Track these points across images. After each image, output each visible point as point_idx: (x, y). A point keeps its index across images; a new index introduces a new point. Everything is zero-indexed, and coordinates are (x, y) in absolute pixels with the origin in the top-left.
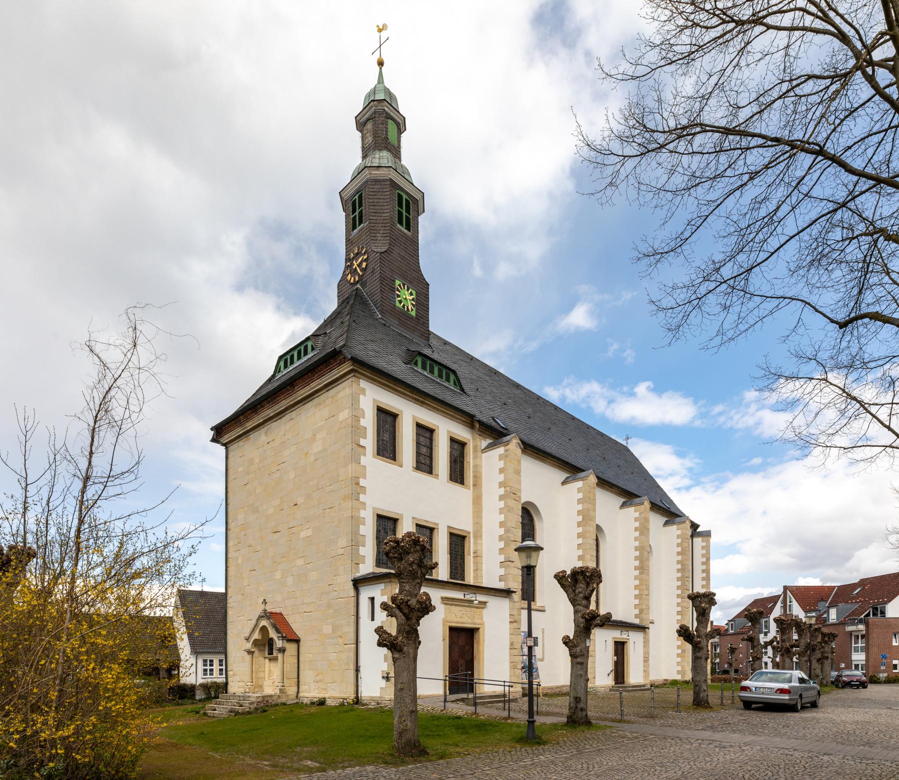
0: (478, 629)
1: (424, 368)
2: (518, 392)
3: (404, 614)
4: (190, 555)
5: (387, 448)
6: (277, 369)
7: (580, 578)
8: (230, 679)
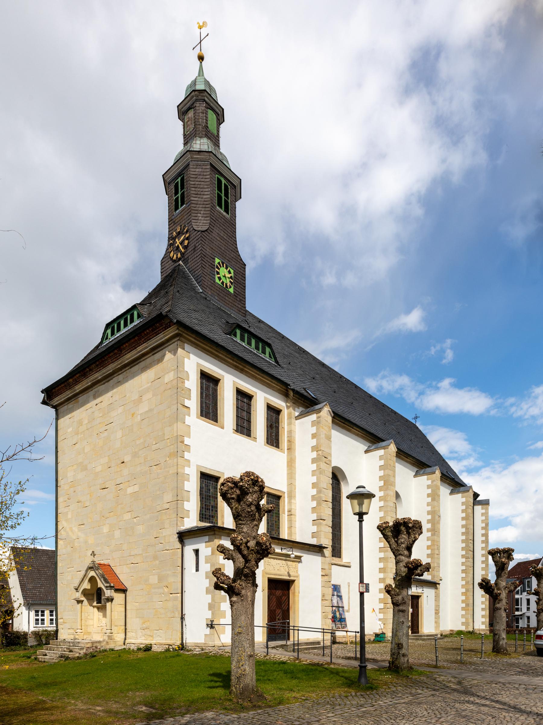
0: (293, 581)
1: (242, 339)
2: (323, 369)
3: (244, 556)
4: (18, 493)
5: (209, 410)
6: (105, 337)
7: (403, 528)
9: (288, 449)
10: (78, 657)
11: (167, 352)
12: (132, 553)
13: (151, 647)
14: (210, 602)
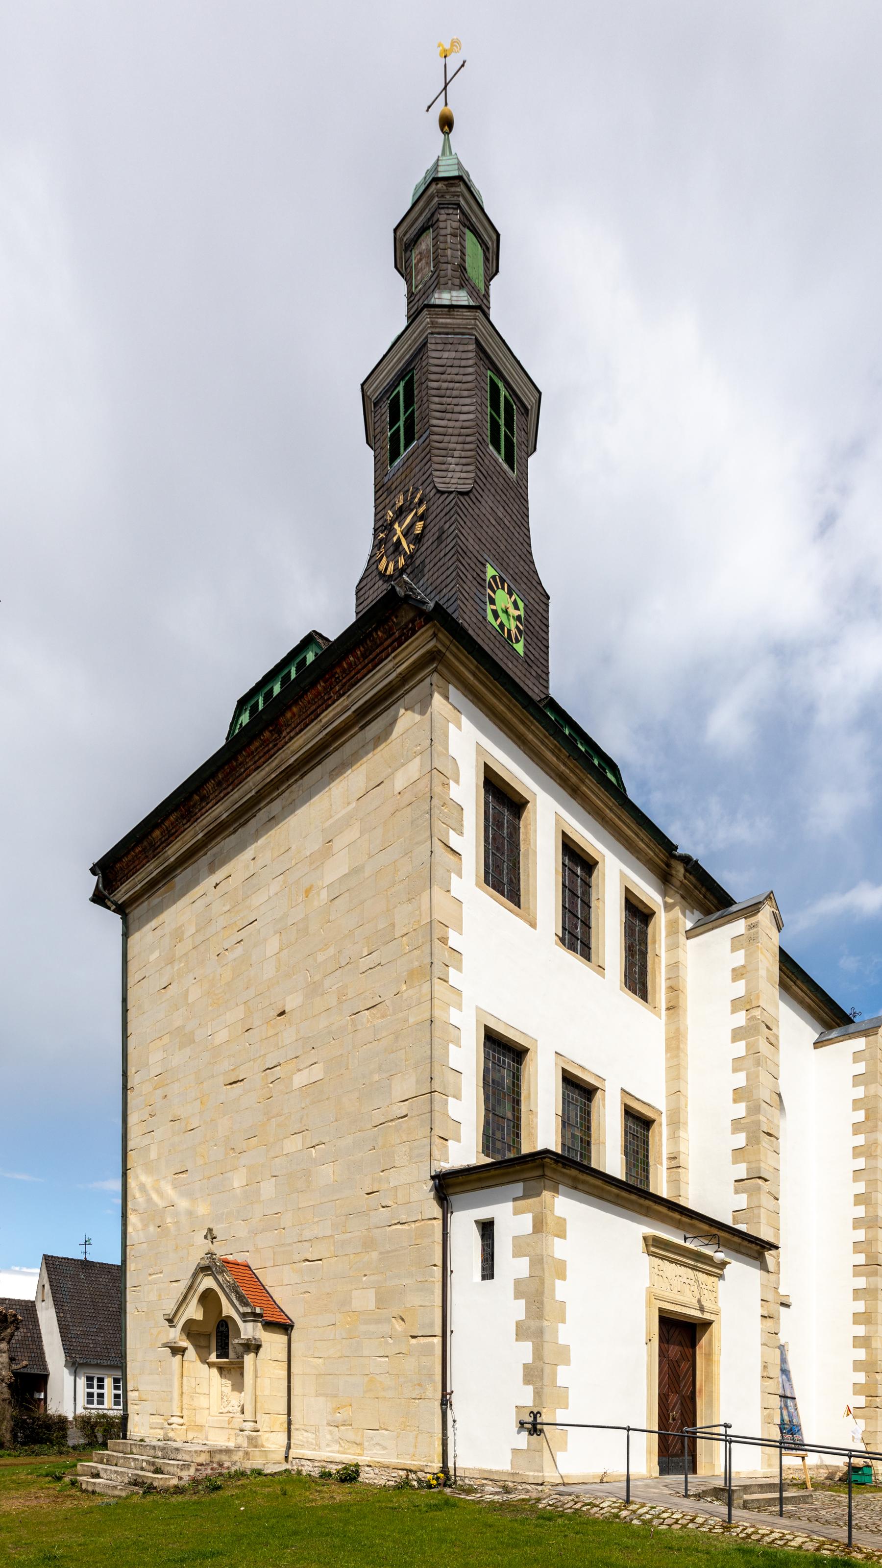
0: (707, 1324)
8: (131, 1409)
9: (668, 1009)
10: (176, 1487)
11: (402, 711)
12: (307, 1234)
13: (357, 1473)
14: (529, 1360)
